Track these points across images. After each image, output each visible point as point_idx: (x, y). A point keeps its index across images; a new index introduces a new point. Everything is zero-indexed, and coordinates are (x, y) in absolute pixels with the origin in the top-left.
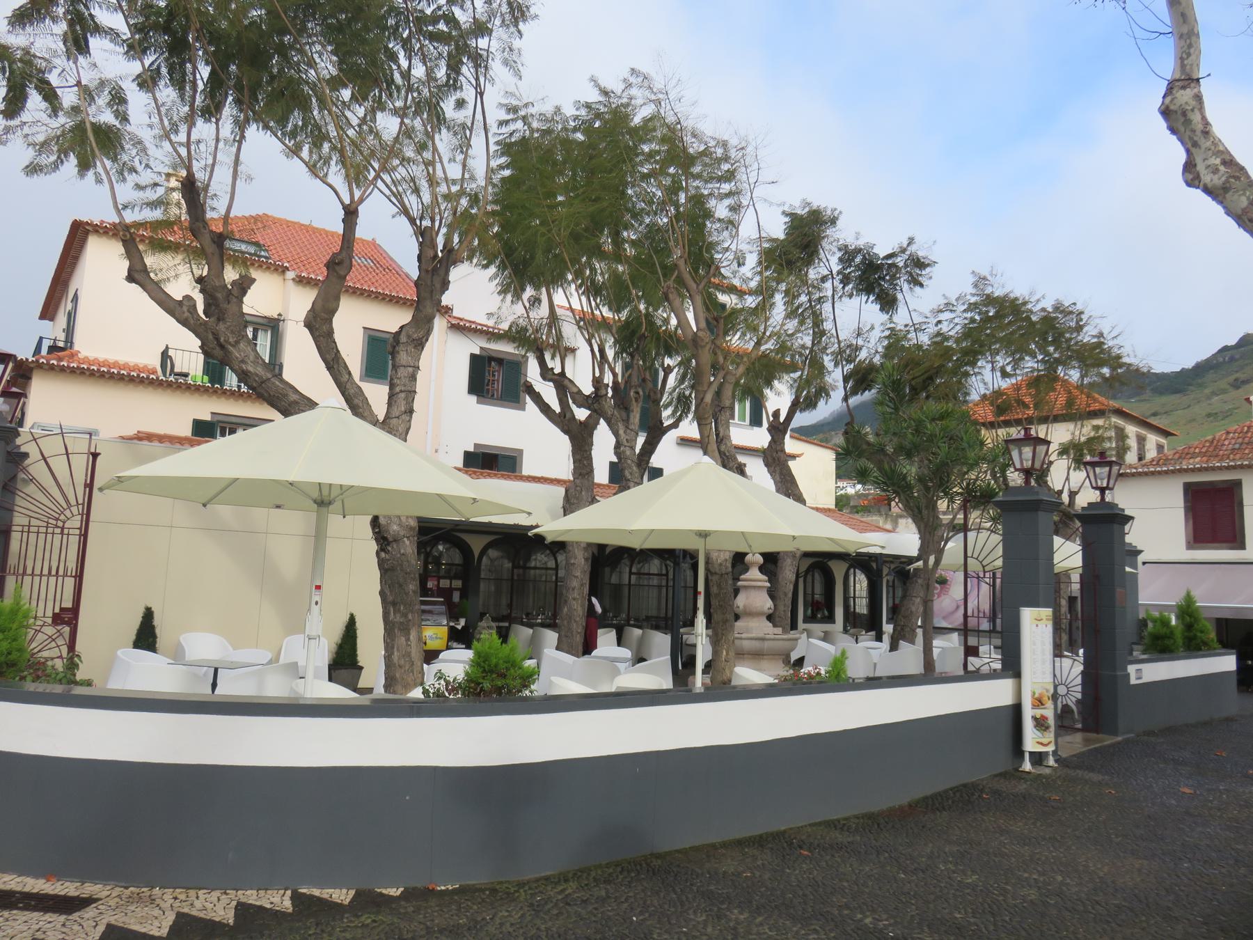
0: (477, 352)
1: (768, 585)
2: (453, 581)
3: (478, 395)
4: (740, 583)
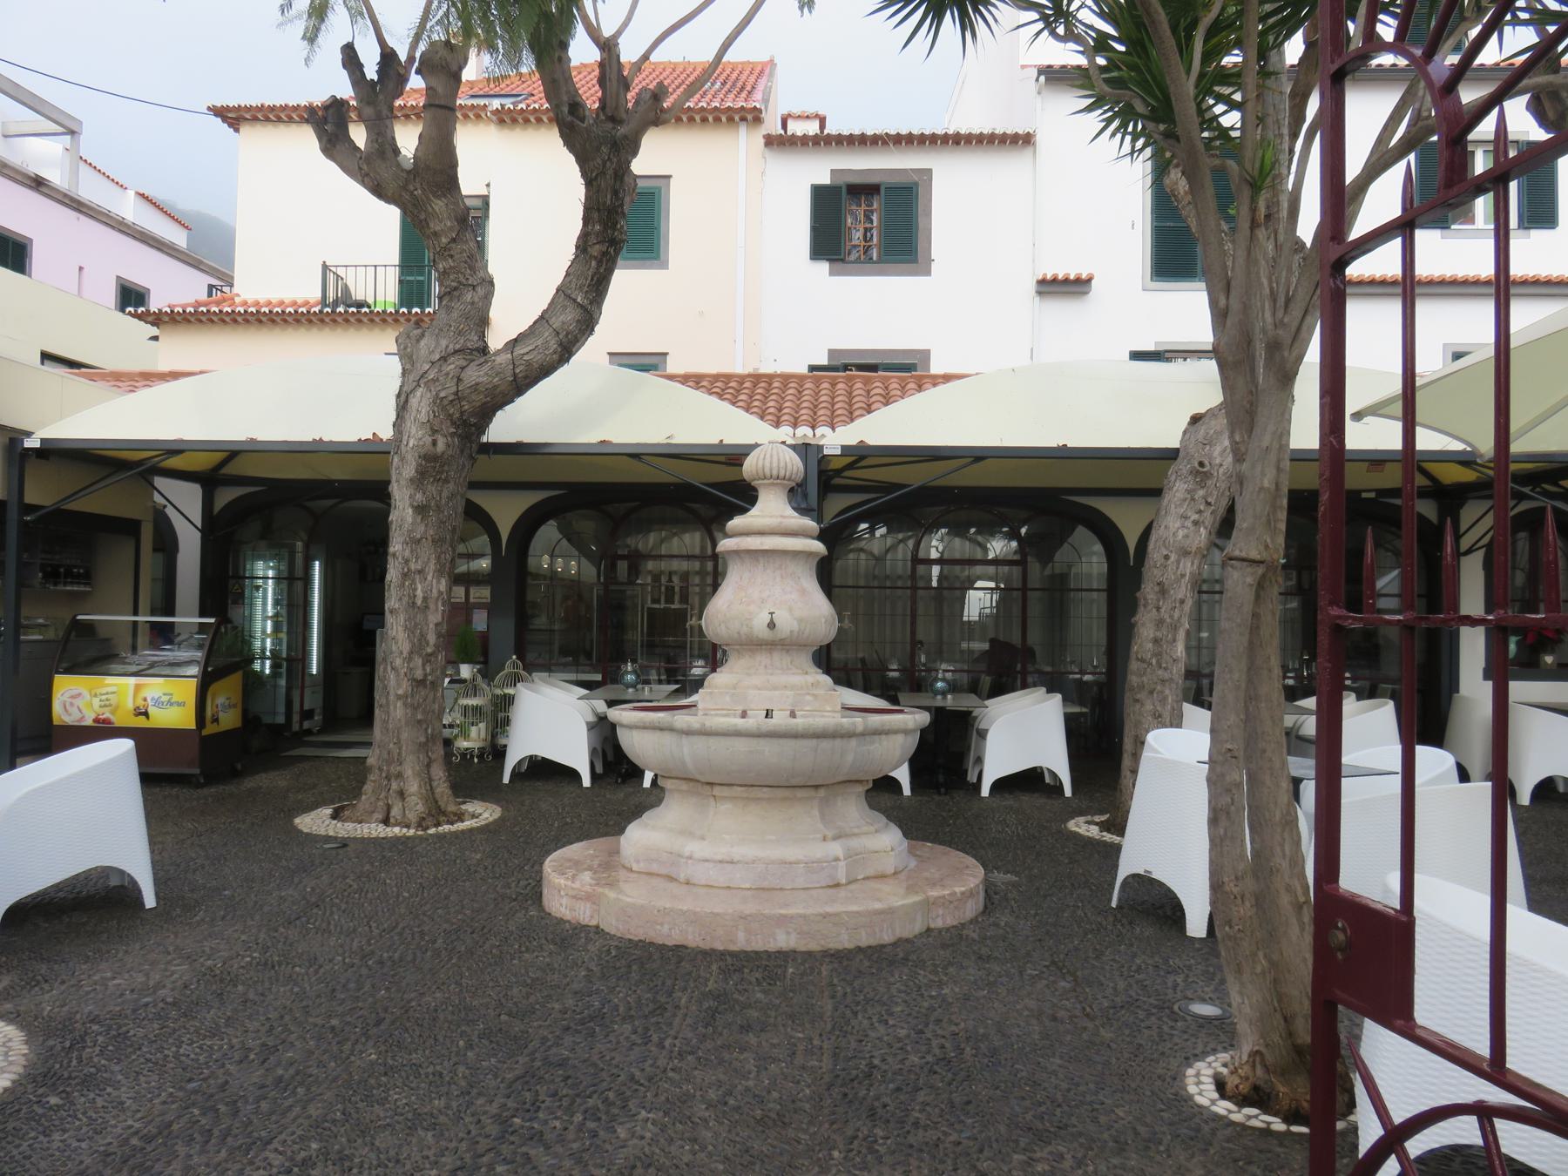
0: (826, 180)
1: (819, 547)
2: (472, 590)
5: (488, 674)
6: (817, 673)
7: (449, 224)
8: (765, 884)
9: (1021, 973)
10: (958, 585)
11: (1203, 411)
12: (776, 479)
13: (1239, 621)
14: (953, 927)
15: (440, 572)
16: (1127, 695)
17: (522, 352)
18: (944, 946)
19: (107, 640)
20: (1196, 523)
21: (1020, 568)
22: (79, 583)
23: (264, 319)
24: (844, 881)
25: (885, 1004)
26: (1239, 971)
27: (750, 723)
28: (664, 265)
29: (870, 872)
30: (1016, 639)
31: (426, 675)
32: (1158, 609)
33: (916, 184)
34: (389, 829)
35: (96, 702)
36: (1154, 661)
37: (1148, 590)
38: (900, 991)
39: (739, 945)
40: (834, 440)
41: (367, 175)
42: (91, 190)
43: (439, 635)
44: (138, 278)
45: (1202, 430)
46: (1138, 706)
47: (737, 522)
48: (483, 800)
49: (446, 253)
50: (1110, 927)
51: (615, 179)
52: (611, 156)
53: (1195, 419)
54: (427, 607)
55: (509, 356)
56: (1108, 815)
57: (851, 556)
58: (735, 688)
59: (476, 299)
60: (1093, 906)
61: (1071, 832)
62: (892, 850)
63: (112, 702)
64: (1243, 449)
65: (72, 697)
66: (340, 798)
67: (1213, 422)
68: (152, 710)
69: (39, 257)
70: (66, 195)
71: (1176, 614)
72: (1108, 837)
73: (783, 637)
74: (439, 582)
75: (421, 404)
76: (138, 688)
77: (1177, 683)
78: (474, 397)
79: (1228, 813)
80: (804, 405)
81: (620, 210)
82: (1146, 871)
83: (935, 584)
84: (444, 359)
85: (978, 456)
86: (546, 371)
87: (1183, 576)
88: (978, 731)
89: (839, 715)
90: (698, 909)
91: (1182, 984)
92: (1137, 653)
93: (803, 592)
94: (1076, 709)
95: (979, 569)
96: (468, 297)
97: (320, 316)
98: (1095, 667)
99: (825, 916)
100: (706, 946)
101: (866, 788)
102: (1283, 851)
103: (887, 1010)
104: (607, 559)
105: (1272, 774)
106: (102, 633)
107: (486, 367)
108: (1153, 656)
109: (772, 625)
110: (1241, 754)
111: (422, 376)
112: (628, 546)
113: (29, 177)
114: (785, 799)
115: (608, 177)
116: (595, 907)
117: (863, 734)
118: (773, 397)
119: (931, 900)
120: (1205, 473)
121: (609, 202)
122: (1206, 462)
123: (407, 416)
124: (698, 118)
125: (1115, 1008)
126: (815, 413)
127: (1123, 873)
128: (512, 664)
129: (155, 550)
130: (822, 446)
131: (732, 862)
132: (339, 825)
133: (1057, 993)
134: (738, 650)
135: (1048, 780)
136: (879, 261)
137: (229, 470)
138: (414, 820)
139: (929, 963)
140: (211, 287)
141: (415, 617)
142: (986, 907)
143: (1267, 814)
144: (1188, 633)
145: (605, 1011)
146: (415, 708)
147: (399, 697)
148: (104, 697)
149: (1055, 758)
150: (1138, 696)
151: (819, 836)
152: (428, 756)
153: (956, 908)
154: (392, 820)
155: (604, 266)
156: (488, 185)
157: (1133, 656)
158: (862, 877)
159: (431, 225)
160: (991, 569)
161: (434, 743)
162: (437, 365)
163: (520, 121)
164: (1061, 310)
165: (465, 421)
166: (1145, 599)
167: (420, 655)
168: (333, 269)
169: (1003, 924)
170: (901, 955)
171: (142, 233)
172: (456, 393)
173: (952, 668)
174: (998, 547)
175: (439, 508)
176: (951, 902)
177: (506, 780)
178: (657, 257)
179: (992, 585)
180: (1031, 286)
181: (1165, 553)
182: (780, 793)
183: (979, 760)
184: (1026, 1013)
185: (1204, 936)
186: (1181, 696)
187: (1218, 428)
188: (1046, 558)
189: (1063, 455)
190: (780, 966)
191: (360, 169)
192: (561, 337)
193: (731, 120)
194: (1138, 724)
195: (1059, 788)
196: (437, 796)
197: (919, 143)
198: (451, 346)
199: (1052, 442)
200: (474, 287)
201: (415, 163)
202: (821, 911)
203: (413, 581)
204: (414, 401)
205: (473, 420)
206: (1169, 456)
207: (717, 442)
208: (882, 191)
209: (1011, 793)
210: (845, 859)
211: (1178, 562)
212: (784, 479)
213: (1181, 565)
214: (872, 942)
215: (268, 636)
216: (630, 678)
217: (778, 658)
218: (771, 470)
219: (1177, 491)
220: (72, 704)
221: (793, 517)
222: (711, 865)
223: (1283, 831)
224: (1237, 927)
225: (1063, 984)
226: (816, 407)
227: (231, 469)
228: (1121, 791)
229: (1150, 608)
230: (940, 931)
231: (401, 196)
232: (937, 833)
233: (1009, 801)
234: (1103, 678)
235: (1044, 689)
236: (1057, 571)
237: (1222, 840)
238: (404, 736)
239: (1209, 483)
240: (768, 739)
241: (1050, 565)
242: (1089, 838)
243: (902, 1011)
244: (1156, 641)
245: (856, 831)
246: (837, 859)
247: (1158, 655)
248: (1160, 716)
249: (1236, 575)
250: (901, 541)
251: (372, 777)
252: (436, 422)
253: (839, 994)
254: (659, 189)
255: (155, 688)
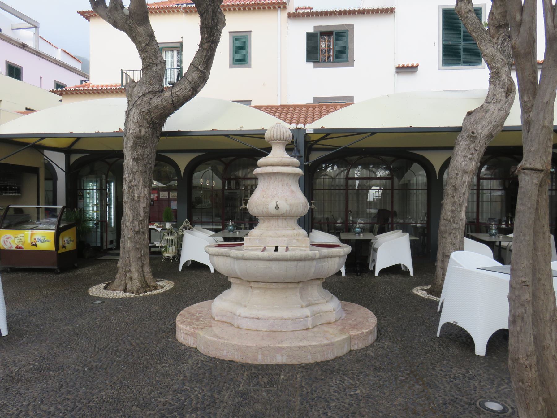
0: (312, 30)
1: (300, 171)
2: (171, 193)
3: (314, 62)
4: (257, 171)
5: (176, 227)
6: (299, 229)
7: (145, 38)
8: (274, 329)
9: (396, 378)
10: (365, 188)
11: (473, 109)
12: (279, 140)
13: (529, 205)
14: (362, 349)
15: (145, 186)
16: (439, 235)
17: (175, 91)
18: (359, 361)
19: (28, 215)
20: (470, 159)
21: (390, 181)
22: (15, 193)
23: (100, 92)
24: (311, 327)
25: (327, 401)
26: (527, 408)
27: (265, 254)
28: (250, 66)
29: (323, 321)
30: (389, 208)
31: (140, 229)
32: (453, 197)
33: (348, 30)
34: (124, 294)
35: (16, 240)
36: (451, 220)
37: (449, 189)
38: (335, 392)
39: (259, 361)
40: (310, 128)
41: (110, 18)
42: (44, 48)
43: (145, 212)
44: (62, 81)
45: (473, 118)
46: (444, 240)
47: (262, 161)
48: (168, 279)
49: (144, 51)
50: (437, 349)
51: (213, 13)
52: (211, 3)
53: (469, 114)
54: (139, 201)
55: (170, 93)
56: (430, 286)
57: (323, 177)
58: (261, 237)
59: (158, 70)
60: (428, 336)
61: (415, 294)
62: (334, 310)
63: (22, 240)
64: (529, 105)
65: (7, 238)
66: (111, 278)
67: (478, 114)
68: (38, 243)
69: (25, 74)
70: (34, 50)
71: (462, 199)
72: (431, 297)
73: (283, 213)
74: (144, 190)
75: (134, 114)
76: (32, 235)
77: (462, 230)
78: (156, 111)
79: (523, 318)
80: (302, 116)
81: (216, 28)
82: (454, 322)
83: (357, 188)
84: (144, 95)
85: (373, 132)
86: (186, 99)
87: (464, 182)
88: (373, 248)
89: (309, 249)
90: (239, 344)
91: (478, 387)
92: (444, 216)
93: (292, 192)
94: (414, 238)
95: (374, 182)
96: (154, 69)
97: (121, 90)
98: (421, 221)
99: (300, 347)
100: (244, 361)
101: (322, 282)
102: (551, 336)
103: (328, 405)
104: (225, 178)
105: (544, 293)
106: (26, 212)
107: (160, 98)
108: (451, 218)
109: (277, 208)
110: (530, 284)
111: (135, 103)
112: (235, 175)
113: (20, 44)
114: (284, 288)
115: (209, 12)
116: (195, 339)
117: (319, 258)
118: (290, 114)
119: (352, 337)
120: (475, 136)
121: (210, 24)
122: (475, 132)
123: (129, 120)
124: (261, 7)
125: (445, 404)
126: (306, 119)
127: (442, 322)
128: (186, 222)
129: (46, 179)
130: (306, 129)
131: (258, 319)
132: (105, 292)
133: (415, 393)
134: (263, 219)
135: (403, 268)
136: (333, 62)
137: (76, 147)
138: (135, 290)
139: (350, 372)
140: (82, 81)
141: (134, 205)
142: (378, 337)
143: (541, 315)
144: (467, 208)
145: (185, 403)
146: (136, 243)
147: (129, 238)
148: (19, 238)
149: (407, 261)
150: (444, 236)
151: (300, 305)
152: (142, 262)
153: (364, 339)
154: (127, 289)
155: (210, 53)
156: (182, 38)
157: (442, 218)
158: (320, 323)
159: (138, 38)
160: (378, 182)
161: (145, 257)
162: (141, 98)
163: (193, 11)
164: (406, 79)
165: (153, 122)
166: (448, 193)
167: (137, 221)
168: (125, 72)
169: (386, 347)
170: (337, 367)
171: (63, 64)
172: (149, 110)
173: (363, 222)
174: (381, 173)
175: (143, 159)
176: (361, 337)
177: (180, 270)
178: (247, 63)
179: (378, 188)
180: (393, 70)
181: (457, 172)
182: (281, 286)
183: (374, 261)
184: (399, 407)
185: (484, 355)
186: (463, 235)
187: (480, 117)
188: (401, 176)
189: (410, 130)
190: (277, 374)
191: (108, 15)
192: (192, 84)
193: (274, 8)
194: (444, 248)
195: (408, 272)
196: (147, 279)
197: (348, 14)
198: (147, 90)
199: (405, 126)
200: (157, 65)
201: (130, 12)
202: (298, 345)
203: (133, 190)
204: (132, 114)
205: (157, 121)
206: (457, 130)
207: (261, 129)
208: (334, 33)
209: (387, 274)
210: (311, 316)
211: (462, 176)
212: (283, 140)
213: (464, 178)
214: (323, 359)
215: (95, 212)
216: (231, 228)
217: (281, 222)
218: (277, 136)
219: (462, 145)
220: (7, 241)
221: (287, 158)
222: (249, 320)
223: (551, 325)
224: (527, 384)
225: (417, 387)
226: (306, 117)
227: (77, 146)
228: (436, 276)
229: (449, 197)
230: (356, 351)
231: (124, 26)
232: (356, 295)
233: (387, 278)
234: (425, 226)
235: (401, 231)
236: (405, 182)
237: (518, 333)
238: (131, 254)
239: (476, 141)
240: (274, 262)
241: (403, 179)
242: (422, 297)
243: (335, 406)
244: (452, 211)
245: (317, 302)
246: (307, 317)
247: (453, 217)
248: (454, 244)
249: (527, 178)
250: (342, 171)
251: (119, 271)
252: (141, 122)
253: (304, 393)
254: (247, 36)
255: (39, 234)
